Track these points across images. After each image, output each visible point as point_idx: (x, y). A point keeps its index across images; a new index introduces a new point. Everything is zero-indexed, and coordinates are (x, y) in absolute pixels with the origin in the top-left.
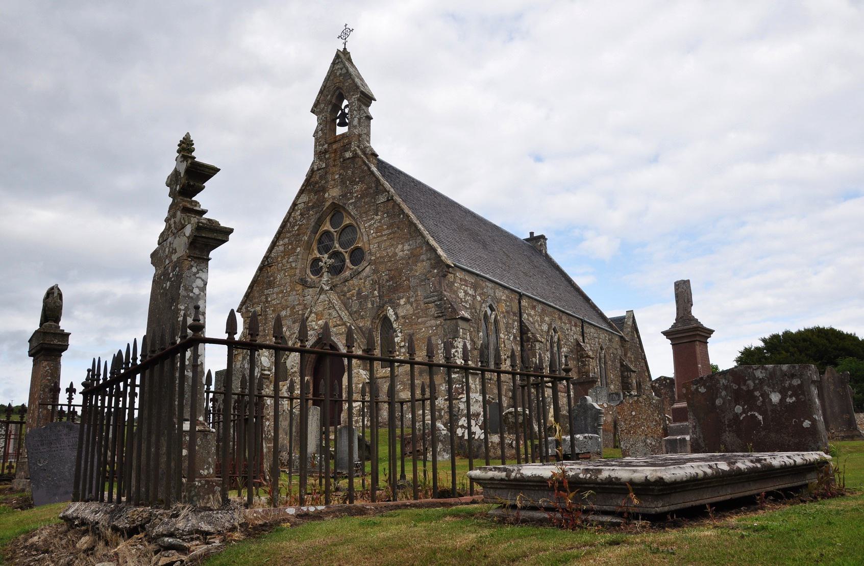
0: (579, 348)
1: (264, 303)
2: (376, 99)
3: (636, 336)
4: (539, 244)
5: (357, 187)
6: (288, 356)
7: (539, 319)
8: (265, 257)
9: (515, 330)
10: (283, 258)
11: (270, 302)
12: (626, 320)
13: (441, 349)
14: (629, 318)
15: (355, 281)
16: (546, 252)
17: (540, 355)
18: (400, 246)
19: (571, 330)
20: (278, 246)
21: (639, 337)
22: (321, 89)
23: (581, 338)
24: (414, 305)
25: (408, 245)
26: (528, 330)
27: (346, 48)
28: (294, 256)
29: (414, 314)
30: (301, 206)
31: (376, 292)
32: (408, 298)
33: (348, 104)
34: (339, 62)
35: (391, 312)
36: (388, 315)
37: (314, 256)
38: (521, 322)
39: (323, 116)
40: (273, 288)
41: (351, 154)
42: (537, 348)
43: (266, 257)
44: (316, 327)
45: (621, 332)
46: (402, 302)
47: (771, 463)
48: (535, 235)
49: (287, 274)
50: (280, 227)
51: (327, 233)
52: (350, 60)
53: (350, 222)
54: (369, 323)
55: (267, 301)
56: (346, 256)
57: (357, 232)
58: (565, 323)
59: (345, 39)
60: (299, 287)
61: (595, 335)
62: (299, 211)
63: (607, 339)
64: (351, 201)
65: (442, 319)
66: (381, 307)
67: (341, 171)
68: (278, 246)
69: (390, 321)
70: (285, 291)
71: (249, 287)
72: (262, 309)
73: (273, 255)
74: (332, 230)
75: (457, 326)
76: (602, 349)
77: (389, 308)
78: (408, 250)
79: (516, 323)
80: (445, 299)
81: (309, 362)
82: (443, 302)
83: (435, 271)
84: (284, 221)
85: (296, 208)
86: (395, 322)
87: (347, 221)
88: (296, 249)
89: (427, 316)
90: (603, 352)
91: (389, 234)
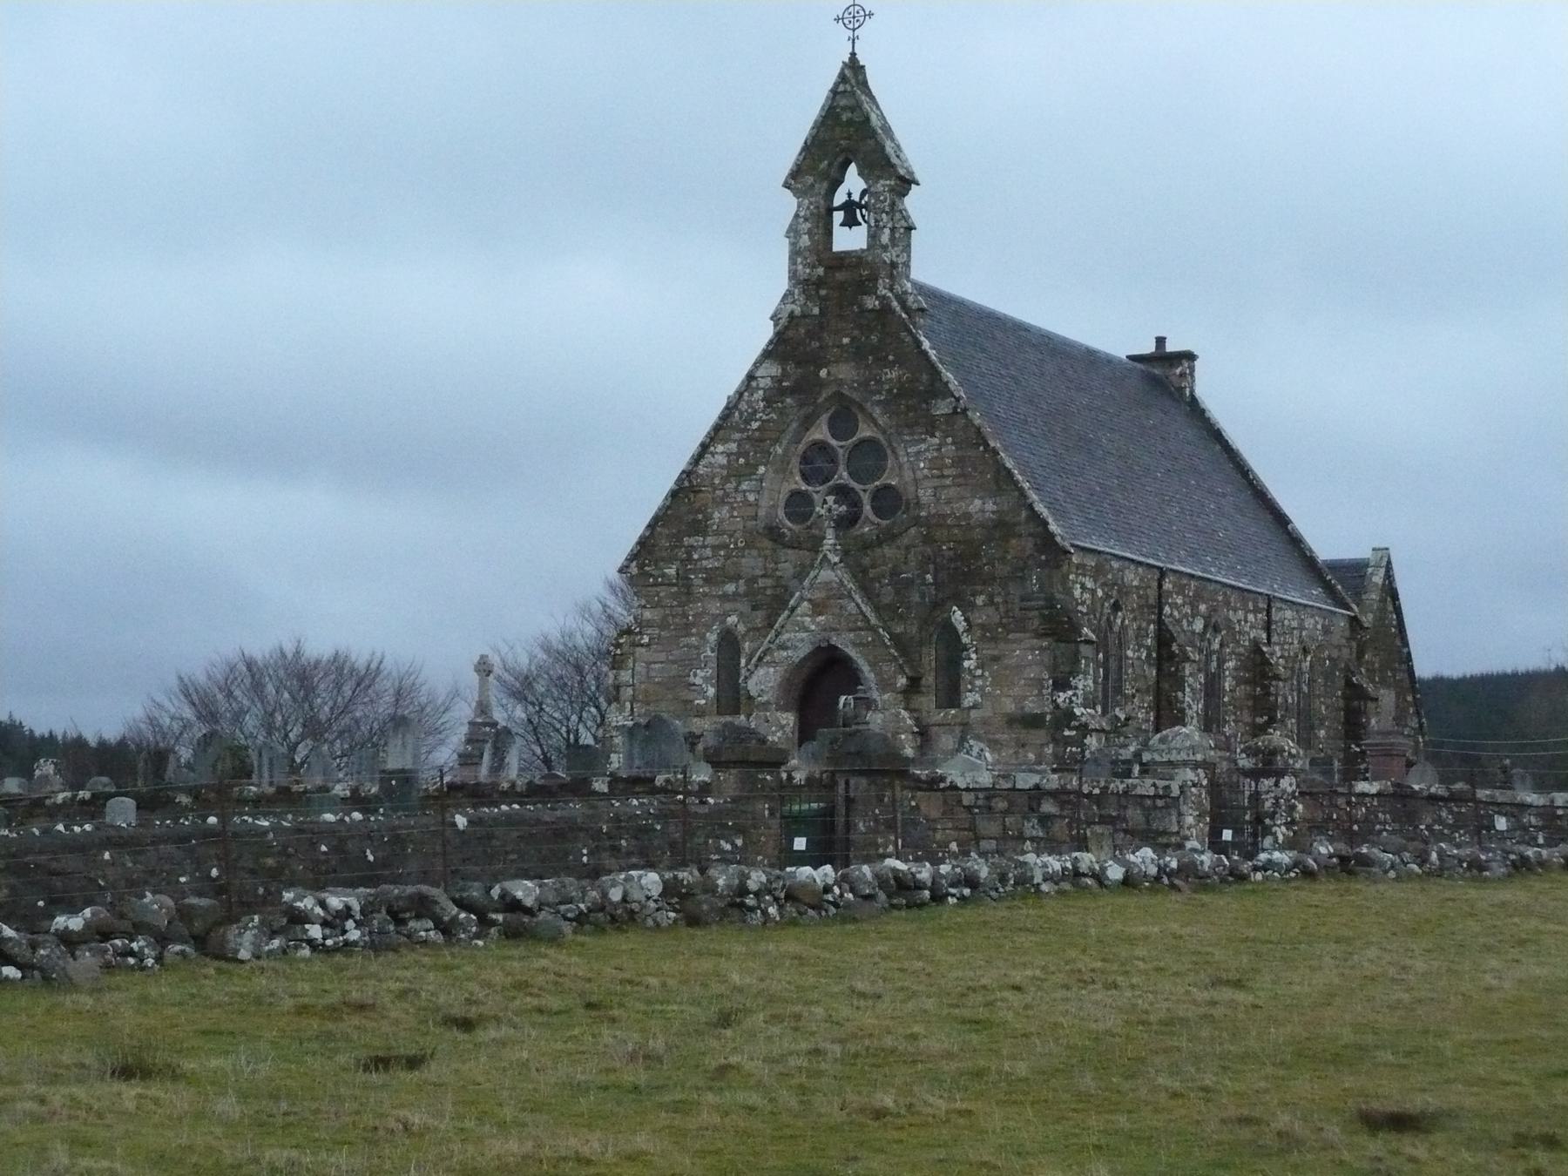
0: (1258, 659)
1: (682, 561)
2: (920, 182)
3: (1391, 608)
4: (1178, 371)
5: (892, 374)
6: (753, 673)
7: (1189, 611)
8: (683, 472)
9: (1149, 640)
10: (726, 479)
11: (696, 561)
12: (1370, 570)
14: (1377, 566)
15: (888, 551)
16: (1192, 392)
17: (1073, 545)
18: (978, 502)
19: (1246, 621)
20: (713, 454)
21: (1398, 610)
22: (806, 143)
23: (1264, 636)
24: (1002, 609)
25: (994, 503)
26: (1173, 639)
27: (856, 51)
28: (751, 480)
29: (1001, 624)
30: (765, 383)
31: (929, 577)
32: (991, 597)
33: (865, 186)
34: (845, 91)
35: (958, 617)
36: (953, 620)
37: (794, 486)
38: (1160, 622)
39: (811, 203)
40: (704, 536)
41: (877, 303)
42: (1187, 672)
43: (687, 474)
44: (813, 627)
45: (1354, 607)
46: (980, 600)
48: (1170, 347)
49: (735, 514)
51: (821, 447)
52: (864, 84)
53: (874, 435)
54: (914, 630)
55: (689, 559)
56: (866, 499)
57: (886, 455)
58: (1235, 610)
59: (854, 30)
60: (767, 543)
61: (1295, 624)
62: (761, 392)
63: (1319, 627)
64: (877, 398)
66: (939, 605)
67: (856, 332)
68: (713, 454)
69: (955, 630)
70: (732, 546)
72: (678, 574)
73: (701, 470)
74: (834, 442)
75: (1077, 653)
76: (1305, 651)
77: (955, 608)
78: (993, 512)
79: (1152, 626)
80: (1059, 606)
83: (1043, 557)
85: (754, 384)
86: (965, 634)
87: (865, 432)
88: (756, 467)
89: (1024, 630)
90: (1309, 658)
91: (955, 477)
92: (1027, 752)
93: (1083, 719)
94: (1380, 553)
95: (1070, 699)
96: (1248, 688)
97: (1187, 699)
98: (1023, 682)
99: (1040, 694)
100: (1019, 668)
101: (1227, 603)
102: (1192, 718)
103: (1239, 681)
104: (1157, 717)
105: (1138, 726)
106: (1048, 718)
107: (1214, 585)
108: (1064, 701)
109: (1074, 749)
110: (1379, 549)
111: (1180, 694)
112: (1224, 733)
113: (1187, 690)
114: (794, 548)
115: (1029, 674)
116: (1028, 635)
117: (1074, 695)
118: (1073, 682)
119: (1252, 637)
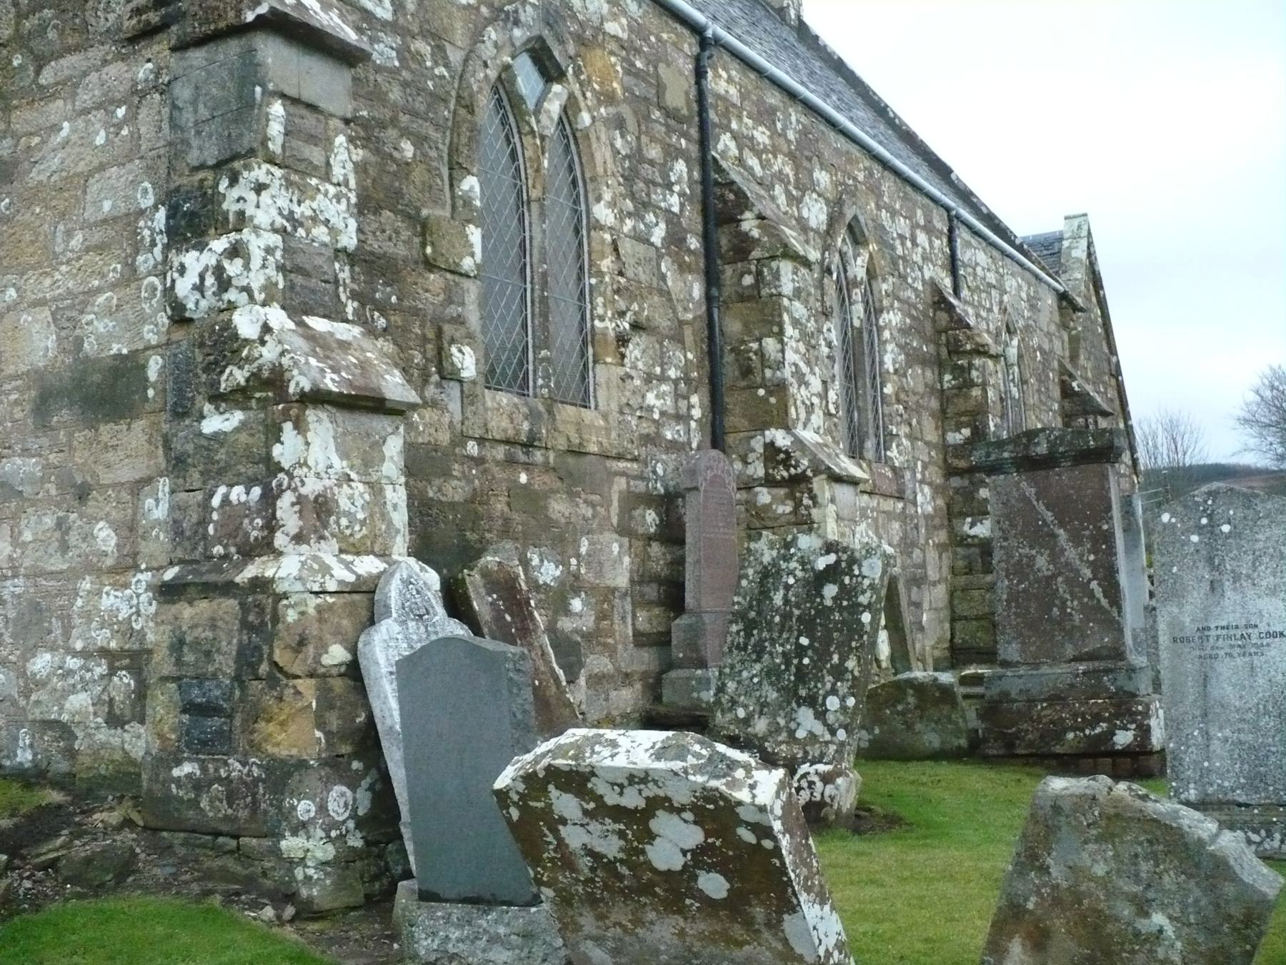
0: (943, 317)
14: (1076, 237)
19: (915, 243)
26: (743, 202)
38: (706, 163)
61: (991, 278)
63: (1024, 295)
65: (160, 48)
92: (93, 520)
93: (268, 353)
94: (1076, 222)
95: (219, 270)
96: (929, 374)
97: (791, 356)
98: (77, 241)
99: (131, 275)
100: (76, 183)
101: (876, 191)
102: (810, 409)
103: (913, 358)
104: (716, 406)
105: (647, 428)
106: (154, 367)
107: (841, 143)
108: (200, 288)
109: (238, 493)
110: (1075, 217)
111: (770, 344)
112: (888, 461)
113: (789, 330)
114: (575, 405)
115: (97, 204)
116: (96, 53)
117: (235, 251)
118: (232, 198)
119: (927, 277)
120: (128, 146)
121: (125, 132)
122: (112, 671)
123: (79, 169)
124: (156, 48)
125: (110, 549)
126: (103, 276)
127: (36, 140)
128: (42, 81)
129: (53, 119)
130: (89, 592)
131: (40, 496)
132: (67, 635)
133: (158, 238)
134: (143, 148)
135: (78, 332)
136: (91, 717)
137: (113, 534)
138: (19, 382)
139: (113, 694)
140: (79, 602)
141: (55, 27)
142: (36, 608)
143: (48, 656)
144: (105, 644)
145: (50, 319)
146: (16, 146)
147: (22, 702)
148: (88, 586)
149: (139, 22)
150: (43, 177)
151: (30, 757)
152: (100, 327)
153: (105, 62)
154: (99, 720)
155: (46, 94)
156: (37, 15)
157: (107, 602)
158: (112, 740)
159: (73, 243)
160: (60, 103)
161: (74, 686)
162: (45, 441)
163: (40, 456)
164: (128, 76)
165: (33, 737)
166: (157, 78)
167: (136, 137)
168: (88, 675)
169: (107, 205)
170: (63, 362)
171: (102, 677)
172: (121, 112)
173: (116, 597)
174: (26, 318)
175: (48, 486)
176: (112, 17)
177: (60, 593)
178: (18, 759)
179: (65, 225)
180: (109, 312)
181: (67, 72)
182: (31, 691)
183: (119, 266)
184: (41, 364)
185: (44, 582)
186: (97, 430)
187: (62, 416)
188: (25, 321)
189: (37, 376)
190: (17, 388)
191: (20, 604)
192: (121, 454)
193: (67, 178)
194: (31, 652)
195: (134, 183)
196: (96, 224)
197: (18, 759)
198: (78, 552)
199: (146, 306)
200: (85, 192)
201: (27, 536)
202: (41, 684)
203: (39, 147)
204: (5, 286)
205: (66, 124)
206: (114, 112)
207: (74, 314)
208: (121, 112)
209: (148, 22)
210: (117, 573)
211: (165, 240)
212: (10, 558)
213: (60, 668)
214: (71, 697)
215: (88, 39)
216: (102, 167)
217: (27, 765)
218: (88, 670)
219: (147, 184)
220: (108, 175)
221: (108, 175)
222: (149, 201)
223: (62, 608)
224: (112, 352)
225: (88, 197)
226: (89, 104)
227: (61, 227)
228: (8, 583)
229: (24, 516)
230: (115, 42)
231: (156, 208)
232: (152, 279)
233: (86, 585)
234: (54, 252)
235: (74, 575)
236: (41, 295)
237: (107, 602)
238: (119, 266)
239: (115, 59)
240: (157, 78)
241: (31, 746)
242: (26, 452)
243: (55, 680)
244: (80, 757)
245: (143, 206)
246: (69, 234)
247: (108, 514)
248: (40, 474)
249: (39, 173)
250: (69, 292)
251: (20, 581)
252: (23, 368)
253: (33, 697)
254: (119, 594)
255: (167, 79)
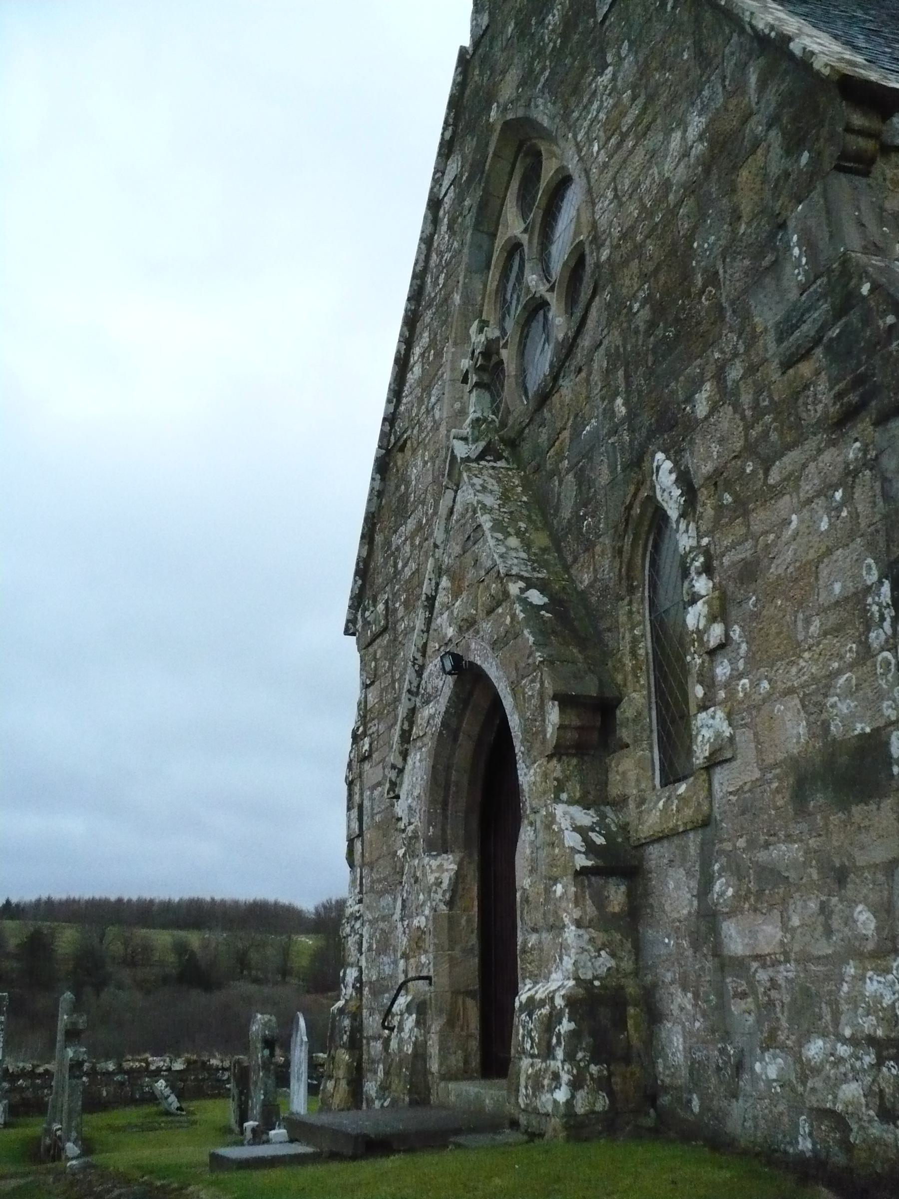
6: (401, 771)
13: (882, 618)
43: (390, 420)
47: (867, 804)
50: (409, 299)
65: (864, 426)
71: (363, 537)
81: (453, 789)
82: (854, 317)
84: (415, 276)
92: (852, 903)
98: (815, 627)
99: (866, 653)
115: (829, 587)
116: (811, 444)
120: (848, 526)
121: (844, 514)
122: (880, 1062)
123: (810, 557)
124: (860, 426)
125: (870, 933)
126: (841, 657)
127: (772, 537)
128: (771, 481)
129: (784, 514)
130: (854, 977)
131: (804, 880)
132: (836, 1022)
133: (886, 612)
134: (862, 525)
135: (824, 716)
136: (864, 1109)
137: (872, 917)
138: (778, 771)
139: (883, 1085)
140: (845, 988)
141: (775, 429)
142: (806, 992)
143: (820, 1043)
144: (872, 1032)
145: (799, 706)
146: (756, 546)
147: (800, 1089)
148: (852, 971)
149: (842, 405)
150: (780, 571)
151: (810, 1146)
152: (844, 708)
153: (820, 451)
154: (872, 1113)
155: (776, 493)
156: (761, 423)
157: (871, 987)
158: (885, 1136)
159: (812, 629)
160: (787, 497)
161: (845, 1075)
162: (804, 826)
163: (801, 841)
164: (839, 459)
165: (811, 1126)
166: (865, 454)
167: (855, 516)
168: (858, 1064)
169: (837, 587)
170: (814, 747)
171: (872, 1066)
172: (838, 495)
173: (879, 982)
174: (779, 707)
175: (809, 870)
176: (820, 407)
177: (828, 978)
178: (800, 1147)
179: (803, 612)
180: (850, 692)
181: (789, 468)
182: (807, 1077)
183: (854, 646)
184: (795, 751)
185: (813, 968)
186: (849, 812)
187: (817, 800)
188: (779, 710)
189: (793, 762)
190: (777, 777)
191: (793, 988)
192: (874, 835)
193: (799, 568)
194: (804, 1038)
195: (859, 561)
196: (829, 608)
197: (800, 1147)
198: (841, 936)
199: (883, 683)
200: (817, 579)
201: (795, 921)
202: (817, 1070)
203: (775, 543)
204: (759, 680)
205: (794, 517)
206: (833, 496)
207: (820, 698)
208: (838, 495)
209: (850, 403)
210: (879, 958)
211: (893, 614)
212: (782, 942)
213: (832, 1055)
214: (844, 1087)
215: (803, 433)
216: (829, 551)
217: (809, 1154)
218: (858, 1059)
219: (870, 561)
220: (834, 558)
221: (834, 558)
222: (874, 577)
223: (830, 993)
224: (856, 733)
225: (821, 582)
226: (811, 494)
227: (801, 616)
228: (782, 968)
229: (792, 901)
230: (825, 430)
231: (880, 583)
232: (886, 654)
233: (850, 970)
234: (797, 640)
235: (837, 960)
236: (789, 684)
237: (871, 987)
238: (854, 646)
239: (827, 446)
240: (865, 454)
241: (810, 1134)
242: (789, 838)
243: (828, 1067)
244: (856, 1152)
245: (869, 583)
246: (808, 622)
247: (866, 897)
248: (802, 859)
249: (777, 566)
250: (813, 678)
251: (791, 966)
252: (781, 756)
253: (810, 1084)
254: (882, 979)
255: (874, 453)
